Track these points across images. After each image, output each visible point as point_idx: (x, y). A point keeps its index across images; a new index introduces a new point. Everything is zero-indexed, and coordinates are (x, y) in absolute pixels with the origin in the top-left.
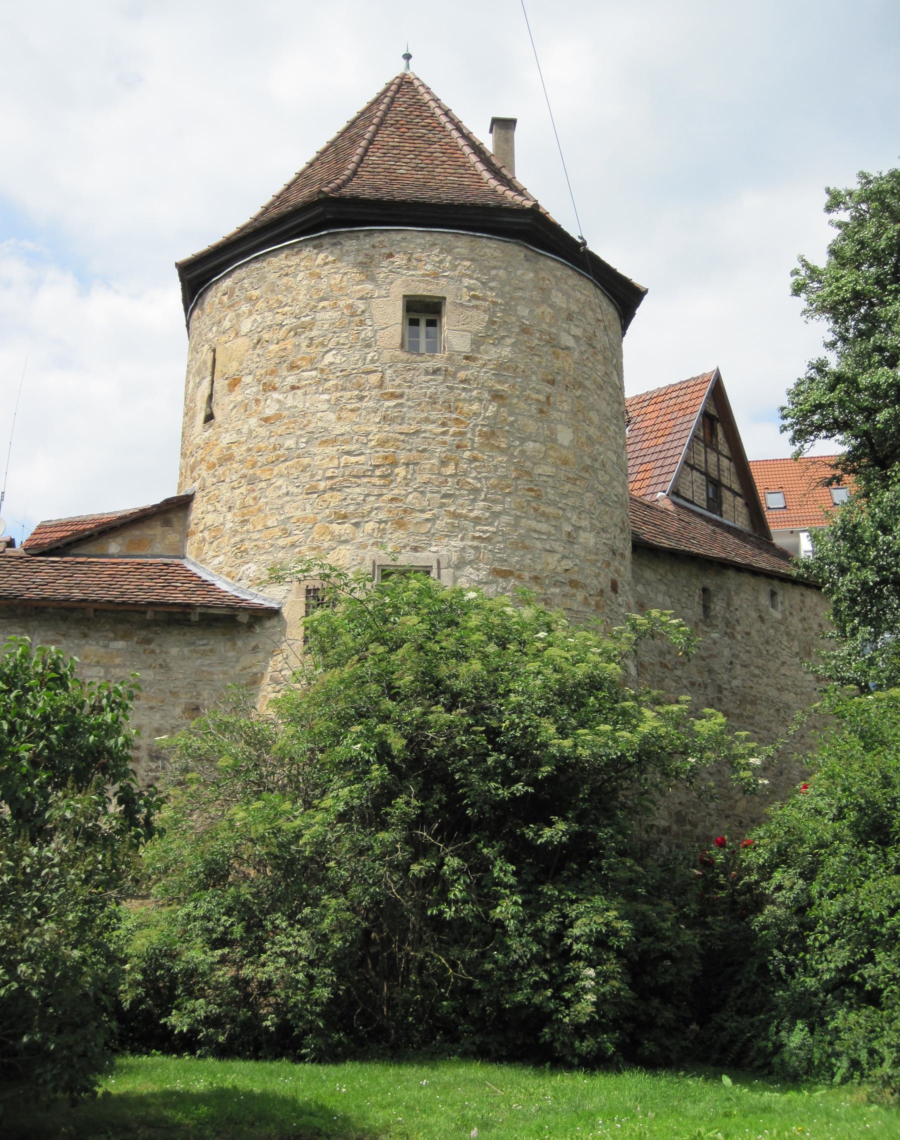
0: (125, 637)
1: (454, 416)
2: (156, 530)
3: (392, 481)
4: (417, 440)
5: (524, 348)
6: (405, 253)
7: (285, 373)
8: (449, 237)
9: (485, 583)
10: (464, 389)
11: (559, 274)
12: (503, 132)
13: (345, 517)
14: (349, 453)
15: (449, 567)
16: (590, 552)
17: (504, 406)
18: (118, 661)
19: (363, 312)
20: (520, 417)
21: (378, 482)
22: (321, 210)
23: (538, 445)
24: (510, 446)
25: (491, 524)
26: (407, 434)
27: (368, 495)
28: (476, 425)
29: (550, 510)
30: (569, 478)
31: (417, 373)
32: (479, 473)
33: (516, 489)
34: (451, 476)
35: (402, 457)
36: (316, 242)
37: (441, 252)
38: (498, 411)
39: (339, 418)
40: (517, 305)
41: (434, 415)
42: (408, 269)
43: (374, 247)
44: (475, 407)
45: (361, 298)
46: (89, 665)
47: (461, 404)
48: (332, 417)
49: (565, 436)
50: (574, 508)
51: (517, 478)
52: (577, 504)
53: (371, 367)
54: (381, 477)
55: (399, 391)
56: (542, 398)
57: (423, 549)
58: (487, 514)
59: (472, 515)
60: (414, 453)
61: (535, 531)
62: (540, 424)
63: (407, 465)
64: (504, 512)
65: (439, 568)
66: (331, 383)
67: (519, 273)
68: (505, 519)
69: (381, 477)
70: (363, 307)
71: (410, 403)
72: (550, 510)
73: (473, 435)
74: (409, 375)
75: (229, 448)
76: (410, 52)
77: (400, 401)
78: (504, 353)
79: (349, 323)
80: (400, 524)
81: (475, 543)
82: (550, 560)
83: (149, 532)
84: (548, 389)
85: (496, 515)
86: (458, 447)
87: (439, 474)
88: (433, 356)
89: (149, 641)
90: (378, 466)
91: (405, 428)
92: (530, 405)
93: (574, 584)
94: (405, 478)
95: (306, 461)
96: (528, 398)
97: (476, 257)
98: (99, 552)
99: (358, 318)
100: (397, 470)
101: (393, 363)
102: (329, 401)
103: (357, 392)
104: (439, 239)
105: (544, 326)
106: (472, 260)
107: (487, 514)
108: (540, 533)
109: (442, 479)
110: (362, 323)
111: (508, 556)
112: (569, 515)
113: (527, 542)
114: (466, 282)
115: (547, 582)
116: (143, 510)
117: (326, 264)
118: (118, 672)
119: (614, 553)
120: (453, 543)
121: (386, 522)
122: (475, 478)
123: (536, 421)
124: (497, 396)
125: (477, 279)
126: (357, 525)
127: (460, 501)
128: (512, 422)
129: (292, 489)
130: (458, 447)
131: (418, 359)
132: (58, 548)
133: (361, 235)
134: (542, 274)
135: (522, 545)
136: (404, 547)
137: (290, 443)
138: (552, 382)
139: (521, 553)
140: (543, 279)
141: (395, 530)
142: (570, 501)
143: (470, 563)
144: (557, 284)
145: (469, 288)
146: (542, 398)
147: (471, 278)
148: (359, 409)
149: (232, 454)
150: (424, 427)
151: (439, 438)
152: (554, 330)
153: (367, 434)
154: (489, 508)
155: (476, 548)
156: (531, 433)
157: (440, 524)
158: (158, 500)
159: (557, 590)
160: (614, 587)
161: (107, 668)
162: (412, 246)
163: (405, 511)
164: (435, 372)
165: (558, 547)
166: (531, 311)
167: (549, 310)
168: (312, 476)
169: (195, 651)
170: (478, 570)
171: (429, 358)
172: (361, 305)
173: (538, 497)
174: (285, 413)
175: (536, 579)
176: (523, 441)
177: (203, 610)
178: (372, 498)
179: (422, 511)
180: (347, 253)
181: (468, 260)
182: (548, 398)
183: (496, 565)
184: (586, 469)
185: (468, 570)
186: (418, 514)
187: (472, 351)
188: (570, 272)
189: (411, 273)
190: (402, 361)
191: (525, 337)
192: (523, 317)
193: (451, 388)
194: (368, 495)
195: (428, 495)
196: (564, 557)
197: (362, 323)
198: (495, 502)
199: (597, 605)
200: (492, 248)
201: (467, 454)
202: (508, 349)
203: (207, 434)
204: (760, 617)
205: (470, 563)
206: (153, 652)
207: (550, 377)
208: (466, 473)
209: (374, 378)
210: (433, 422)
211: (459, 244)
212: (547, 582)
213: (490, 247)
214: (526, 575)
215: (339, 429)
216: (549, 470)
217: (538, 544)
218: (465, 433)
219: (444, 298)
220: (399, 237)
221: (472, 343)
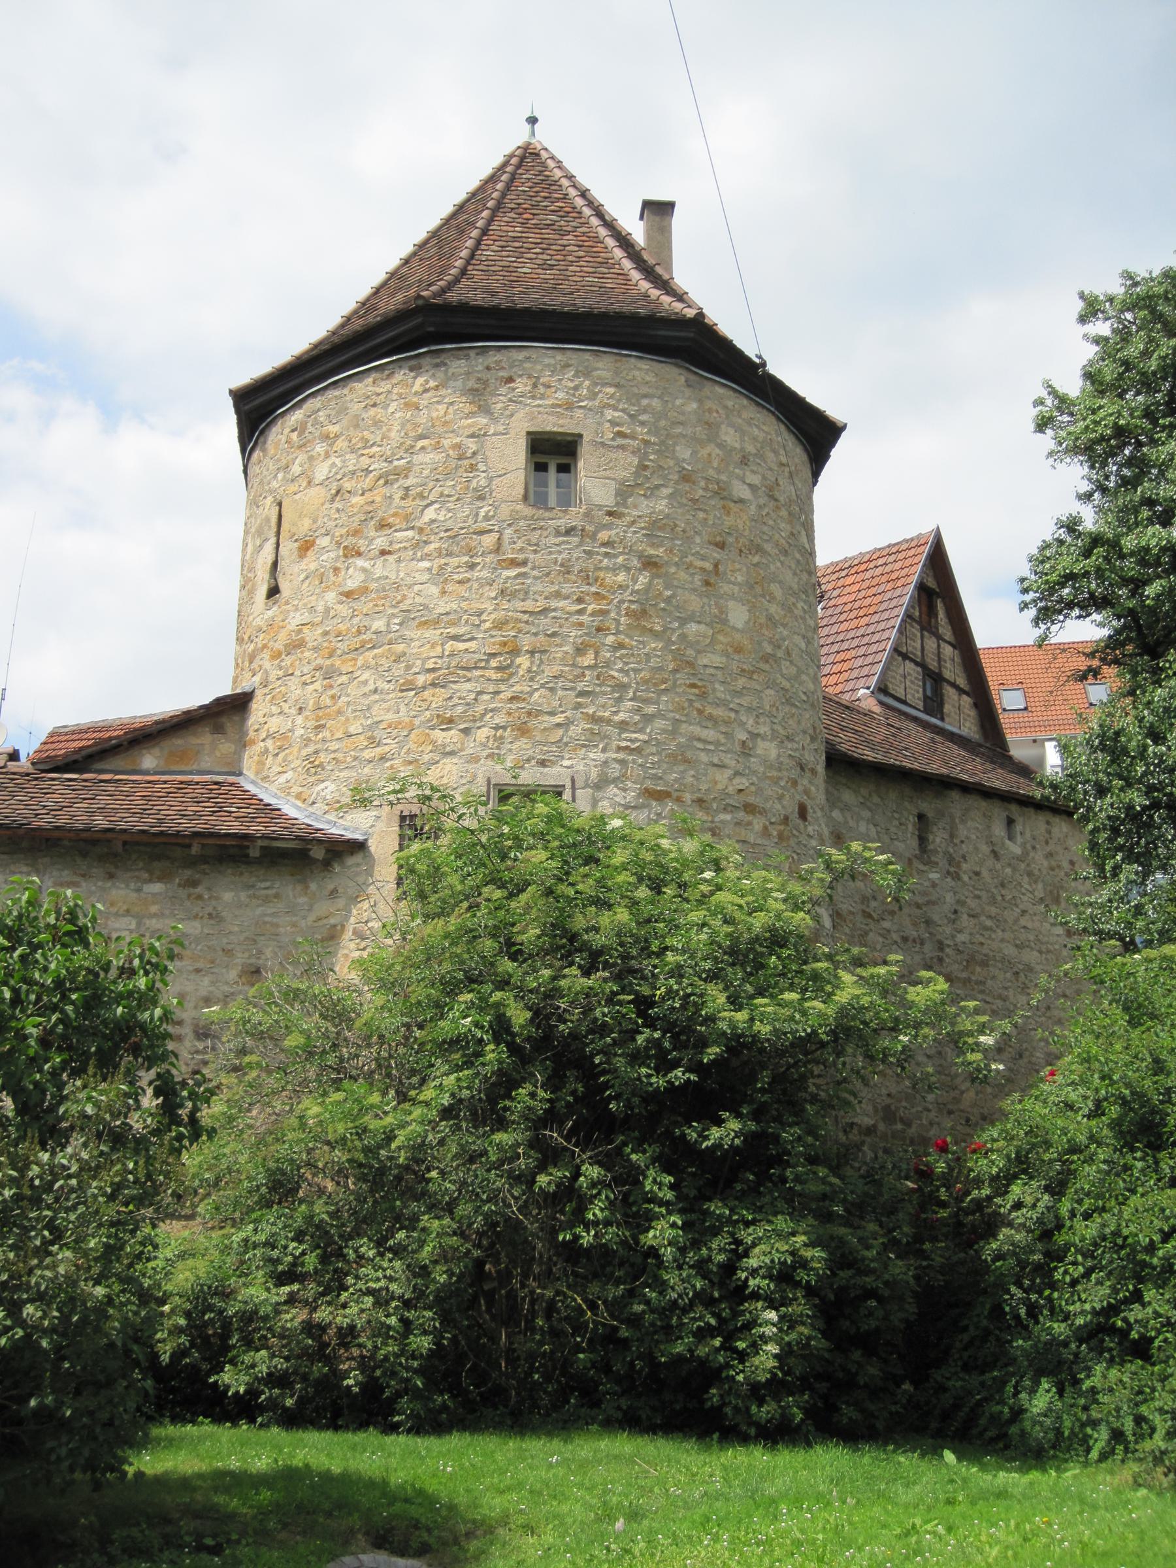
1: (593, 589)
2: (203, 738)
3: (512, 674)
4: (544, 621)
5: (684, 501)
6: (529, 377)
7: (372, 534)
8: (587, 356)
9: (635, 807)
10: (606, 554)
11: (730, 404)
12: (657, 219)
13: (451, 721)
14: (455, 638)
15: (587, 786)
17: (659, 577)
18: (154, 909)
19: (474, 453)
22: (420, 320)
23: (702, 627)
25: (641, 731)
26: (531, 613)
27: (480, 693)
28: (622, 602)
29: (719, 712)
30: (743, 670)
31: (545, 533)
32: (626, 664)
33: (675, 685)
34: (588, 667)
35: (526, 642)
36: (413, 362)
37: (576, 375)
38: (650, 583)
39: (444, 592)
41: (567, 588)
42: (533, 397)
43: (488, 368)
44: (621, 577)
45: (472, 436)
46: (117, 915)
47: (602, 574)
48: (434, 590)
49: (738, 616)
51: (675, 671)
52: (755, 704)
53: (485, 525)
55: (521, 557)
56: (708, 566)
57: (553, 763)
58: (637, 718)
59: (617, 718)
60: (541, 637)
61: (699, 739)
62: (705, 600)
63: (532, 653)
64: (659, 715)
65: (573, 788)
66: (432, 546)
67: (678, 402)
68: (660, 723)
69: (498, 669)
70: (474, 447)
71: (535, 573)
72: (719, 712)
73: (618, 614)
75: (300, 631)
77: (523, 570)
78: (659, 508)
79: (457, 468)
80: (523, 731)
81: (621, 756)
82: (718, 777)
84: (716, 554)
85: (648, 719)
86: (599, 630)
87: (574, 665)
88: (565, 512)
89: (194, 884)
90: (494, 655)
93: (749, 808)
94: (529, 671)
95: (400, 648)
98: (130, 768)
99: (467, 461)
100: (518, 660)
102: (429, 570)
103: (466, 559)
104: (573, 358)
105: (711, 472)
106: (617, 386)
107: (637, 718)
108: (705, 742)
109: (577, 671)
111: (664, 772)
112: (744, 719)
113: (689, 754)
114: (610, 414)
115: (715, 806)
116: (187, 713)
117: (426, 391)
118: (154, 923)
119: (802, 769)
120: (592, 755)
121: (504, 728)
122: (621, 671)
123: (700, 596)
124: (650, 564)
125: (623, 411)
126: (466, 731)
130: (599, 630)
131: (547, 514)
132: (75, 762)
133: (472, 353)
134: (709, 404)
135: (681, 758)
136: (528, 760)
137: (379, 624)
138: (721, 546)
139: (681, 768)
140: (710, 411)
142: (745, 701)
143: (615, 781)
144: (727, 417)
145: (613, 423)
146: (708, 566)
147: (615, 409)
148: (469, 580)
149: (303, 639)
150: (554, 604)
151: (574, 619)
153: (480, 613)
154: (639, 710)
155: (622, 762)
156: (693, 612)
157: (574, 731)
159: (728, 817)
160: (803, 813)
161: (140, 919)
162: (539, 367)
163: (529, 713)
164: (569, 532)
165: (729, 760)
166: (694, 453)
167: (718, 451)
168: (408, 668)
169: (255, 896)
170: (625, 790)
171: (560, 514)
172: (471, 445)
173: (703, 696)
174: (373, 586)
175: (700, 802)
176: (683, 621)
177: (265, 843)
178: (486, 697)
179: (552, 714)
181: (611, 385)
182: (716, 566)
183: (649, 784)
184: (766, 658)
185: (612, 790)
186: (546, 718)
187: (617, 504)
188: (745, 402)
190: (525, 518)
191: (687, 487)
192: (684, 460)
193: (589, 553)
194: (480, 693)
195: (560, 693)
196: (737, 773)
198: (646, 701)
199: (781, 836)
200: (642, 371)
201: (610, 639)
202: (665, 502)
203: (270, 613)
204: (993, 852)
205: (615, 781)
207: (718, 539)
208: (608, 664)
209: (489, 540)
210: (566, 598)
211: (600, 365)
212: (715, 806)
213: (640, 369)
214: (688, 797)
216: (718, 660)
217: (704, 757)
218: (607, 612)
219: (580, 436)
220: (521, 355)
221: (617, 495)
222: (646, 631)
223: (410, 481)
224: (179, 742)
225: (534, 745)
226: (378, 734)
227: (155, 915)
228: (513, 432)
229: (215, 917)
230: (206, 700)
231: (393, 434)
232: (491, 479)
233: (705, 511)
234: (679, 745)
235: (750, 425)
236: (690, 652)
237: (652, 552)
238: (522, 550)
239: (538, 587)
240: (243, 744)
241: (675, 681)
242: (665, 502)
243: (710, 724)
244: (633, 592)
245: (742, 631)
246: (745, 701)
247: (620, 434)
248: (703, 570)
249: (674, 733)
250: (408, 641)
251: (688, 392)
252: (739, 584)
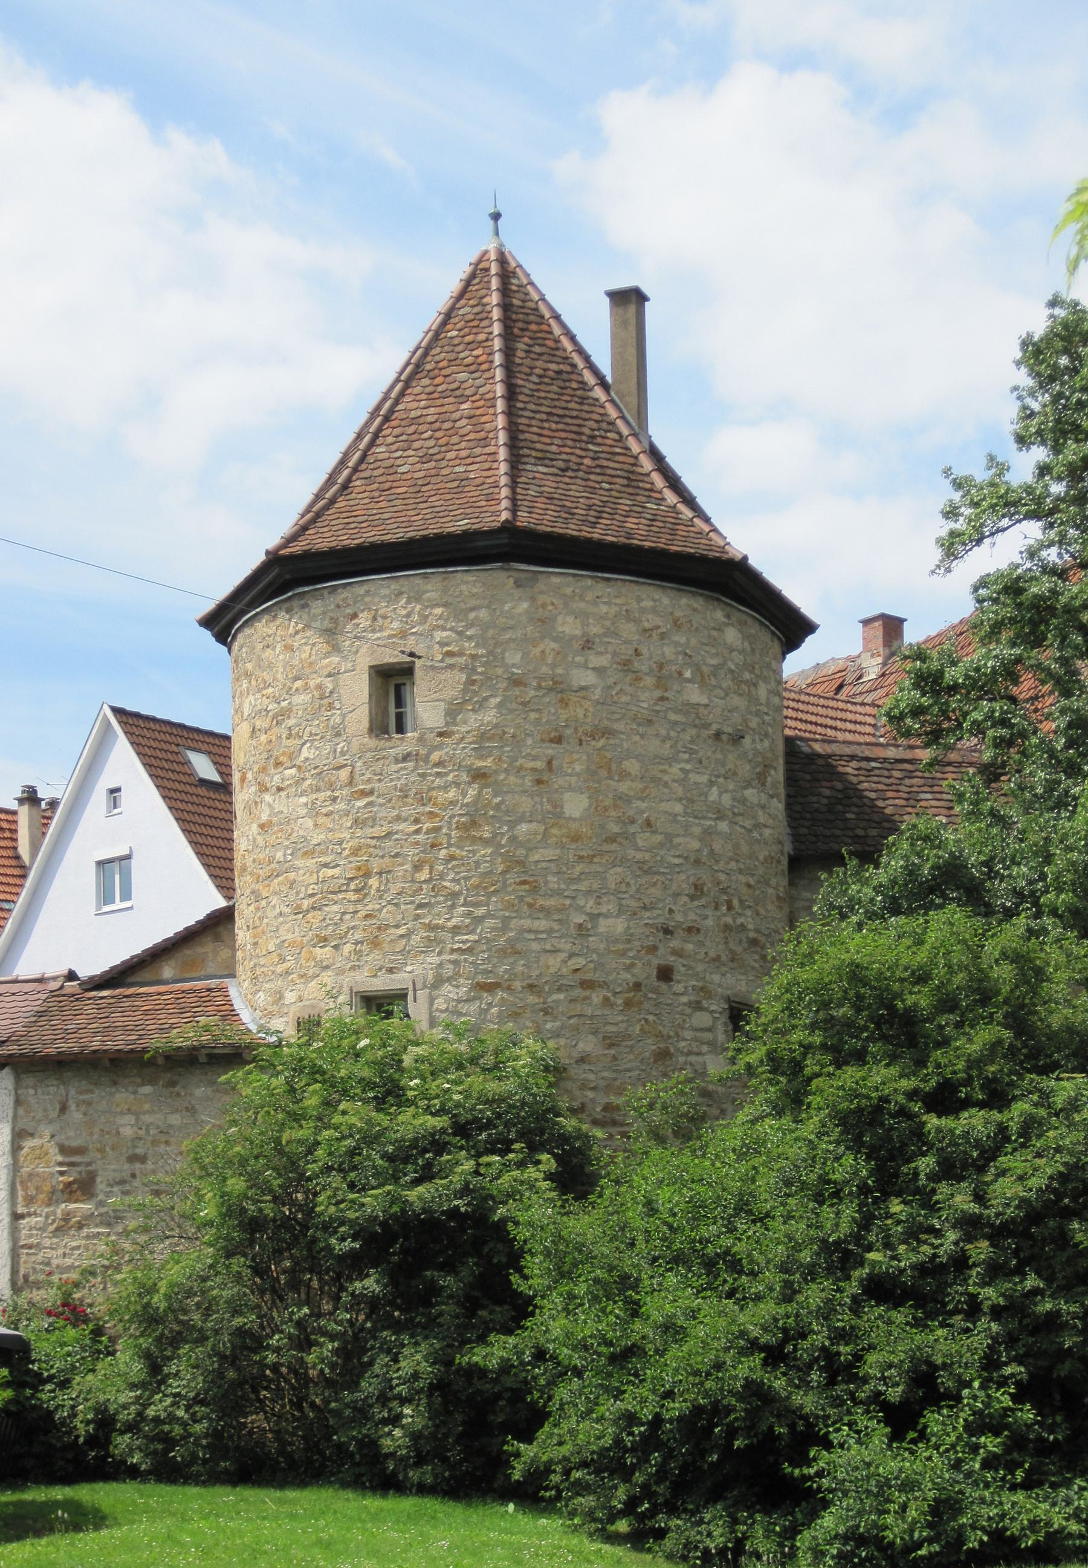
0: (151, 1082)
1: (428, 809)
2: (206, 947)
3: (366, 895)
4: (389, 843)
5: (514, 706)
6: (370, 610)
7: (273, 771)
9: (466, 1001)
10: (438, 774)
11: (568, 591)
12: (620, 310)
14: (326, 865)
15: (425, 987)
16: (616, 941)
17: (486, 786)
18: (147, 1107)
19: (331, 692)
20: (508, 797)
21: (352, 896)
22: (277, 571)
23: (534, 825)
25: (472, 932)
27: (344, 913)
28: (452, 817)
29: (551, 902)
30: (581, 857)
31: (387, 762)
32: (458, 873)
33: (505, 885)
34: (425, 881)
35: (376, 865)
36: (287, 605)
37: (408, 602)
38: (480, 792)
41: (406, 811)
42: (374, 631)
43: (338, 606)
44: (452, 794)
45: (329, 675)
46: (122, 1113)
47: (434, 793)
48: (310, 823)
49: (575, 805)
50: (589, 892)
51: (504, 873)
52: (595, 886)
53: (341, 760)
54: (357, 891)
55: (369, 787)
56: (539, 764)
58: (468, 921)
60: (387, 859)
61: (530, 931)
62: (537, 799)
63: (380, 874)
64: (488, 915)
65: (415, 990)
66: (308, 782)
67: (506, 608)
68: (490, 923)
69: (357, 891)
70: (330, 686)
71: (381, 800)
72: (551, 902)
73: (449, 829)
76: (501, 208)
77: (370, 799)
78: (487, 719)
79: (320, 707)
80: (375, 944)
81: (454, 957)
82: (551, 962)
83: (200, 950)
84: (550, 750)
86: (433, 846)
87: (413, 881)
88: (402, 739)
89: (172, 1084)
90: (351, 879)
91: (377, 831)
94: (378, 891)
95: (292, 876)
96: (521, 769)
98: (154, 978)
99: (326, 700)
100: (371, 881)
101: (363, 750)
102: (306, 804)
103: (329, 793)
106: (446, 605)
107: (468, 921)
108: (537, 932)
109: (416, 886)
110: (331, 707)
111: (494, 966)
112: (582, 903)
113: (519, 946)
114: (439, 635)
115: (547, 988)
117: (297, 633)
118: (147, 1118)
120: (429, 960)
121: (362, 942)
122: (453, 880)
123: (532, 796)
124: (479, 776)
125: (451, 629)
126: (336, 947)
127: (436, 910)
128: (498, 805)
130: (433, 846)
131: (388, 744)
132: (113, 978)
133: (326, 592)
134: (541, 599)
135: (512, 951)
136: (380, 969)
137: (279, 855)
138: (559, 740)
139: (511, 960)
142: (583, 886)
143: (449, 979)
144: (566, 605)
145: (442, 644)
146: (539, 764)
147: (444, 629)
150: (396, 828)
151: (412, 839)
154: (470, 913)
155: (456, 963)
156: (524, 813)
157: (415, 939)
159: (561, 996)
160: (665, 974)
161: (137, 1114)
162: (377, 600)
163: (379, 928)
164: (406, 758)
165: (565, 945)
166: (525, 655)
167: (553, 645)
168: (298, 893)
169: (217, 1091)
170: (457, 987)
171: (398, 743)
172: (329, 685)
176: (513, 825)
177: (208, 1051)
178: (348, 917)
179: (397, 926)
180: (314, 618)
181: (438, 605)
182: (549, 762)
183: (480, 979)
184: (612, 839)
185: (447, 988)
186: (393, 930)
187: (447, 724)
188: (589, 582)
189: (378, 635)
190: (370, 750)
191: (517, 691)
192: (514, 665)
193: (423, 776)
194: (344, 913)
196: (571, 955)
197: (331, 707)
198: (476, 905)
199: (628, 1004)
200: (467, 582)
201: (443, 853)
202: (493, 713)
205: (449, 979)
206: (178, 1095)
207: (552, 735)
208: (442, 876)
209: (344, 774)
210: (405, 820)
211: (429, 587)
212: (547, 988)
213: (467, 583)
214: (518, 985)
215: (317, 838)
216: (550, 853)
217: (535, 946)
218: (440, 828)
221: (446, 715)
222: (474, 840)
223: (291, 722)
224: (188, 952)
226: (284, 952)
227: (148, 1112)
228: (358, 668)
230: (201, 916)
231: (279, 676)
232: (344, 716)
233: (538, 710)
235: (595, 604)
236: (521, 852)
237: (481, 764)
238: (369, 781)
239: (383, 814)
240: (234, 950)
241: (505, 882)
243: (541, 915)
244: (463, 805)
245: (580, 819)
246: (583, 886)
251: (517, 593)
252: (578, 775)
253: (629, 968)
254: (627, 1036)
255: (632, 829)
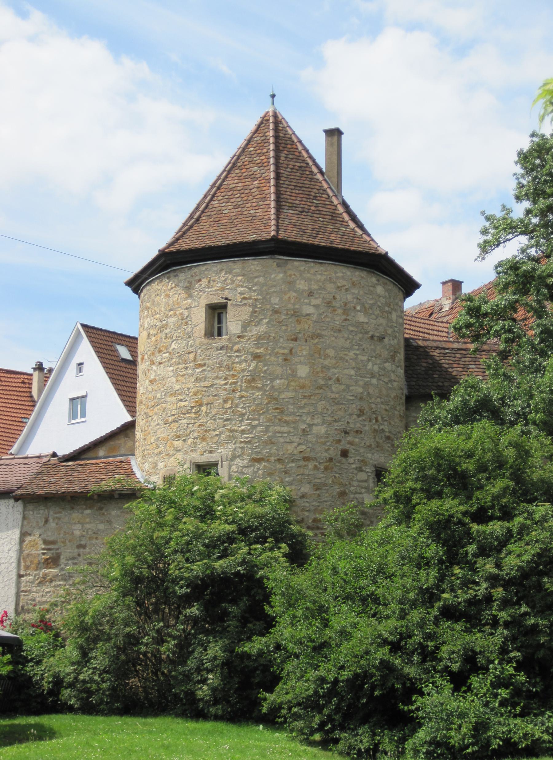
0: (91, 508)
1: (231, 373)
3: (200, 415)
4: (212, 390)
5: (275, 323)
8: (231, 264)
9: (247, 467)
10: (237, 356)
11: (302, 268)
12: (330, 139)
13: (179, 437)
14: (181, 400)
15: (227, 460)
16: (321, 437)
17: (260, 362)
18: (88, 520)
21: (193, 415)
23: (282, 381)
24: (264, 385)
25: (251, 433)
26: (207, 387)
27: (189, 424)
29: (290, 418)
30: (305, 396)
32: (245, 404)
33: (268, 410)
34: (229, 408)
35: (205, 400)
36: (168, 275)
37: (226, 274)
38: (257, 365)
39: (177, 381)
40: (270, 298)
41: (221, 374)
42: (208, 288)
43: (192, 276)
44: (243, 365)
45: (186, 309)
47: (235, 365)
50: (308, 413)
51: (267, 404)
52: (311, 410)
53: (190, 349)
54: (195, 413)
55: (203, 362)
56: (286, 351)
57: (215, 452)
58: (249, 427)
59: (240, 429)
60: (211, 397)
61: (279, 432)
62: (284, 368)
63: (207, 404)
64: (259, 425)
65: (222, 462)
66: (174, 360)
67: (272, 276)
68: (260, 428)
69: (195, 413)
71: (209, 369)
72: (290, 418)
73: (242, 382)
74: (208, 353)
76: (275, 93)
78: (261, 329)
79: (181, 324)
80: (203, 439)
81: (242, 445)
84: (292, 344)
85: (254, 427)
86: (233, 391)
89: (101, 509)
90: (193, 407)
92: (278, 357)
93: (306, 459)
94: (206, 413)
95: (164, 405)
96: (277, 353)
97: (246, 273)
99: (184, 320)
101: (201, 344)
103: (184, 365)
104: (224, 266)
106: (243, 275)
107: (249, 427)
108: (283, 433)
109: (224, 411)
111: (261, 450)
112: (305, 419)
113: (273, 440)
114: (240, 289)
115: (286, 461)
116: (96, 440)
117: (172, 288)
118: (88, 526)
120: (229, 447)
121: (197, 438)
122: (242, 408)
124: (257, 357)
125: (246, 287)
126: (184, 440)
127: (234, 422)
129: (161, 422)
130: (233, 391)
131: (213, 341)
132: (75, 456)
133: (186, 269)
134: (289, 272)
135: (270, 442)
137: (159, 395)
138: (296, 340)
140: (290, 276)
141: (201, 442)
142: (306, 410)
143: (239, 456)
144: (301, 275)
145: (241, 294)
147: (242, 287)
148: (185, 374)
150: (216, 382)
151: (223, 388)
152: (297, 306)
153: (189, 389)
155: (242, 448)
156: (278, 375)
158: (119, 425)
159: (294, 465)
160: (345, 454)
161: (82, 524)
163: (206, 431)
164: (222, 348)
165: (296, 439)
166: (281, 299)
168: (167, 414)
169: (123, 512)
170: (243, 460)
173: (282, 412)
174: (157, 378)
176: (272, 381)
177: (119, 492)
178: (191, 425)
179: (214, 430)
180: (180, 281)
181: (240, 275)
182: (291, 350)
183: (254, 456)
184: (320, 388)
185: (238, 461)
186: (212, 432)
187: (242, 332)
189: (211, 289)
190: (205, 344)
191: (276, 316)
192: (275, 304)
193: (230, 357)
194: (189, 424)
195: (218, 421)
196: (299, 444)
197: (186, 324)
198: (253, 419)
199: (326, 468)
201: (238, 394)
202: (264, 327)
205: (239, 456)
206: (103, 514)
207: (293, 337)
208: (237, 406)
209: (192, 356)
210: (220, 378)
211: (236, 267)
212: (286, 461)
214: (272, 459)
215: (177, 387)
216: (290, 394)
217: (281, 440)
218: (237, 382)
220: (203, 268)
222: (254, 388)
225: (208, 444)
227: (88, 523)
229: (109, 522)
231: (162, 309)
232: (192, 328)
233: (286, 325)
234: (269, 437)
236: (276, 394)
237: (258, 351)
238: (204, 359)
239: (210, 375)
240: (134, 442)
242: (264, 327)
243: (285, 425)
244: (248, 371)
245: (305, 378)
247: (245, 298)
248: (283, 354)
249: (267, 431)
250: (166, 402)
252: (305, 356)
253: (327, 451)
254: (325, 485)
255: (330, 382)
